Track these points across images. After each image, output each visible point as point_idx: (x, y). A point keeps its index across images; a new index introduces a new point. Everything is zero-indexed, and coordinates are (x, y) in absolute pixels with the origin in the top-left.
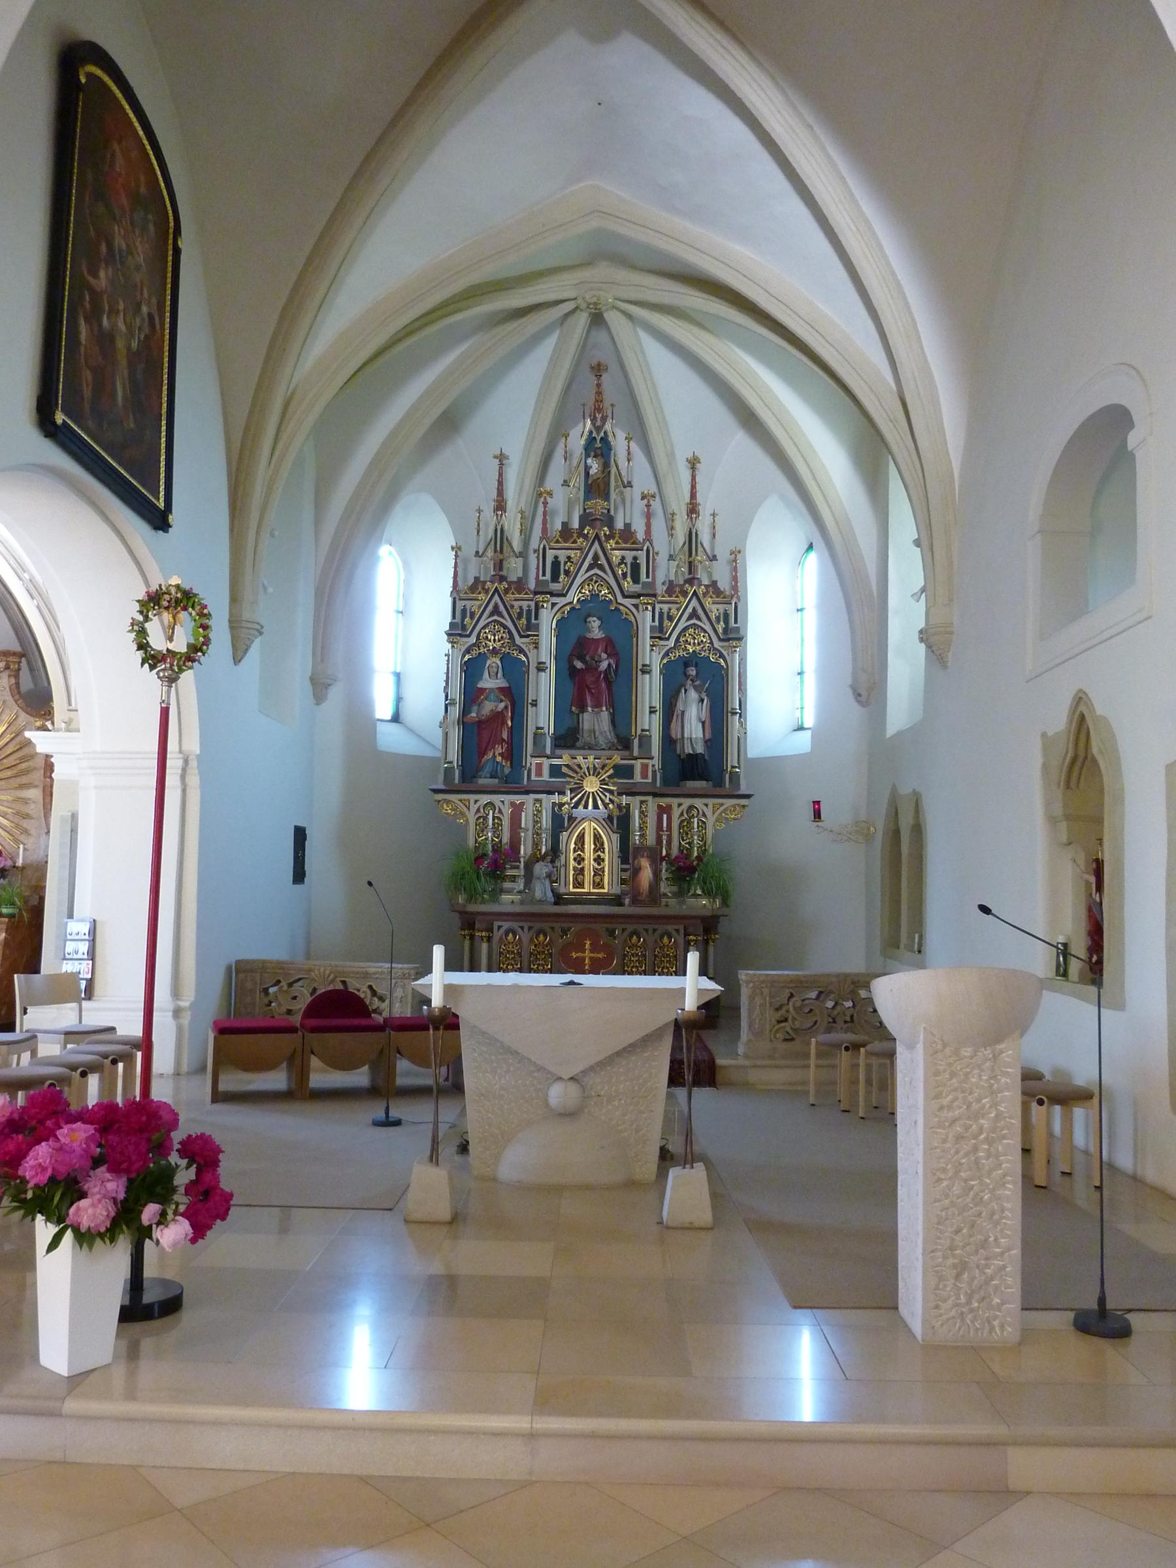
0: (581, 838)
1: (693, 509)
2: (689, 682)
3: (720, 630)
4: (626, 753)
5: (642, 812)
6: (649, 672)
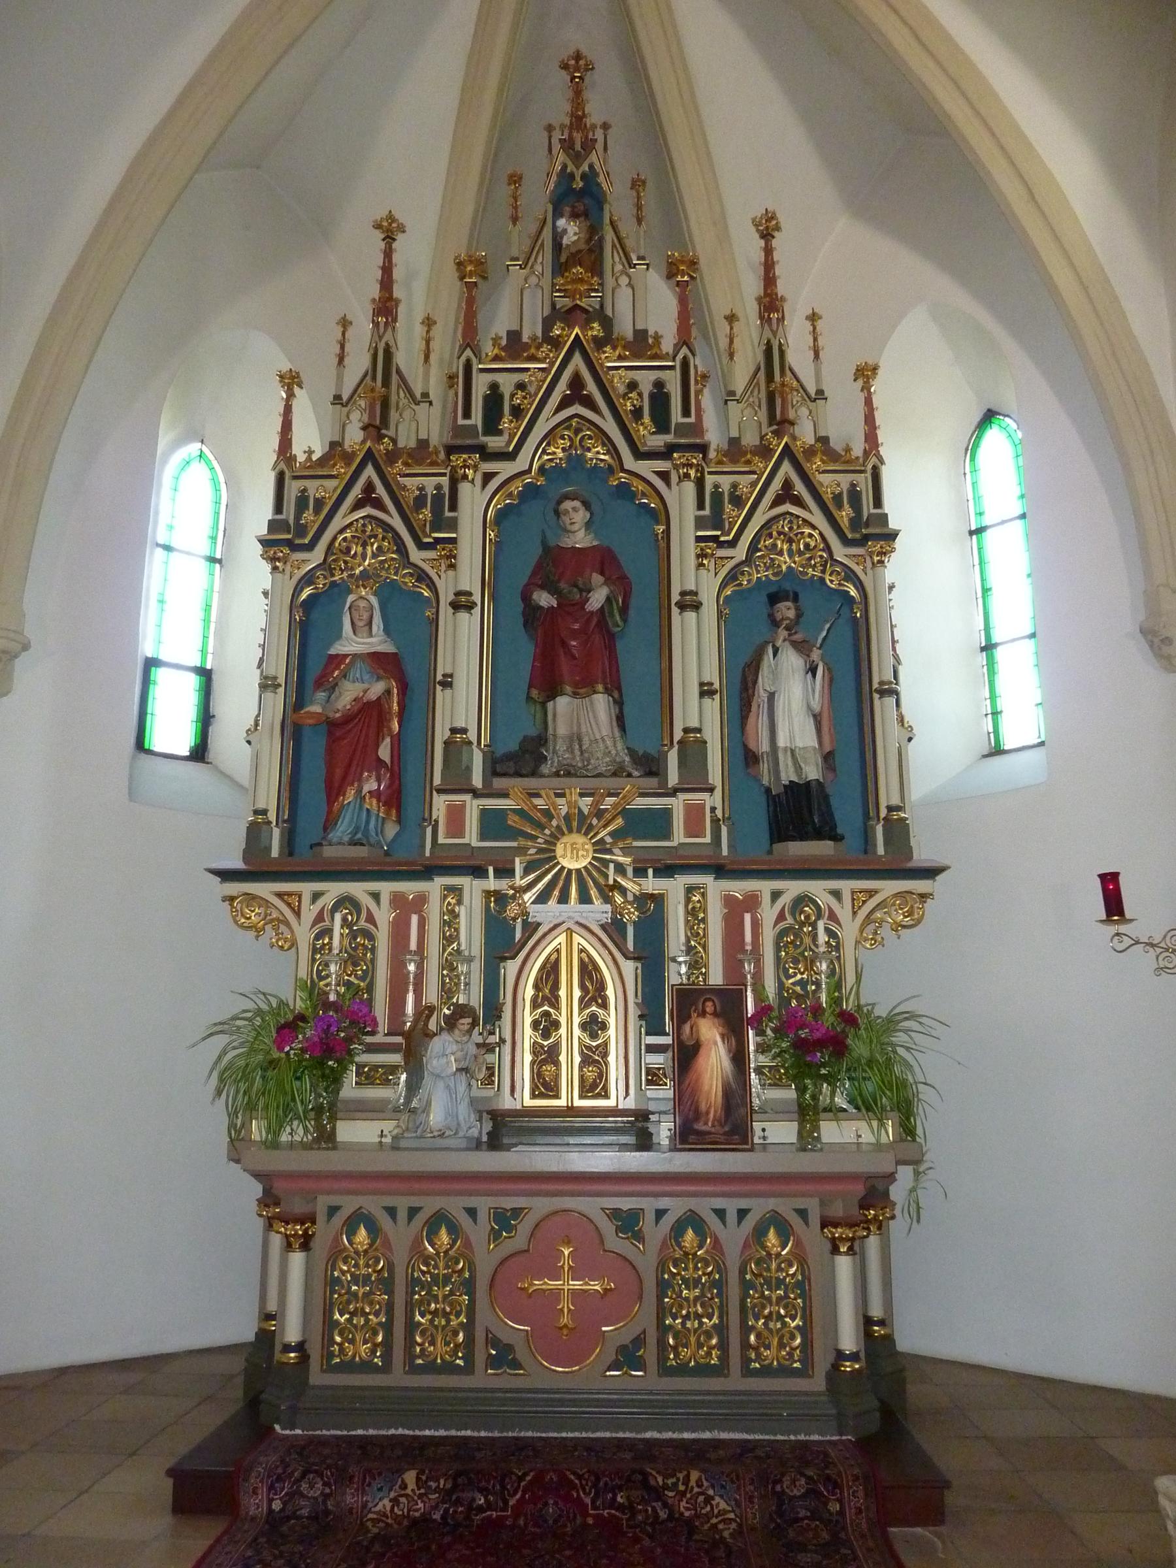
0: (551, 971)
1: (771, 305)
2: (782, 633)
3: (845, 523)
4: (653, 782)
5: (691, 913)
6: (697, 606)
